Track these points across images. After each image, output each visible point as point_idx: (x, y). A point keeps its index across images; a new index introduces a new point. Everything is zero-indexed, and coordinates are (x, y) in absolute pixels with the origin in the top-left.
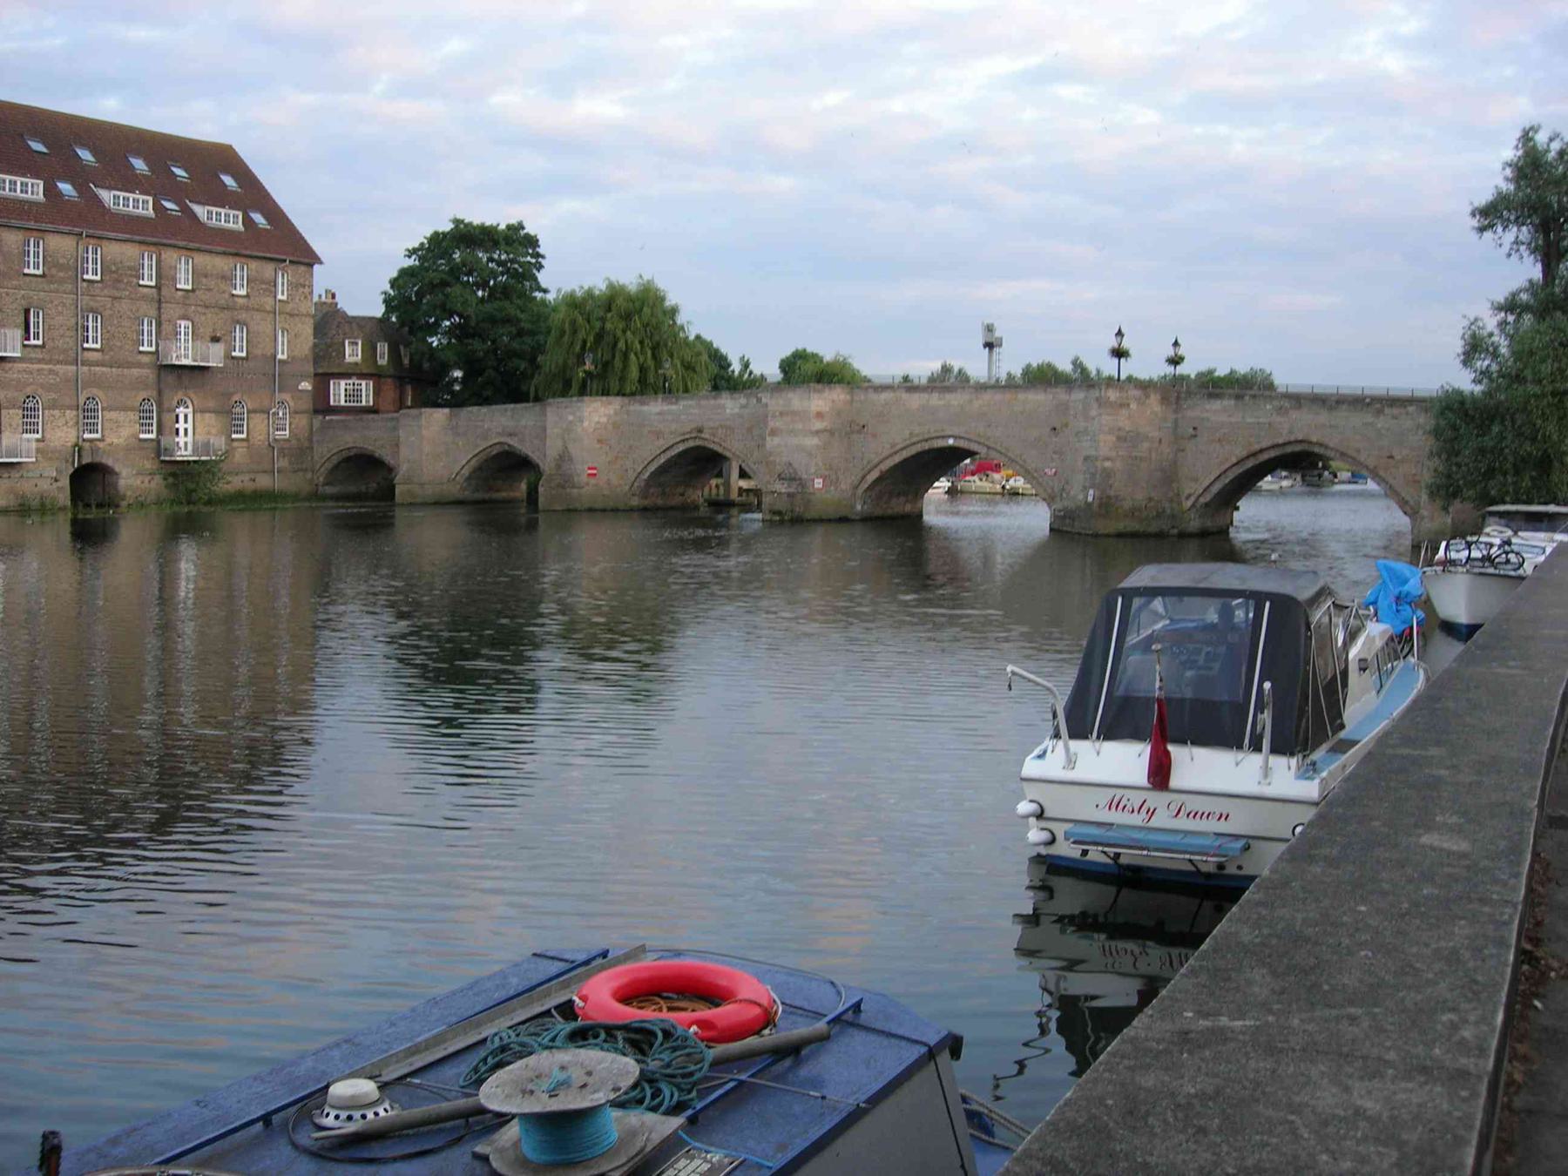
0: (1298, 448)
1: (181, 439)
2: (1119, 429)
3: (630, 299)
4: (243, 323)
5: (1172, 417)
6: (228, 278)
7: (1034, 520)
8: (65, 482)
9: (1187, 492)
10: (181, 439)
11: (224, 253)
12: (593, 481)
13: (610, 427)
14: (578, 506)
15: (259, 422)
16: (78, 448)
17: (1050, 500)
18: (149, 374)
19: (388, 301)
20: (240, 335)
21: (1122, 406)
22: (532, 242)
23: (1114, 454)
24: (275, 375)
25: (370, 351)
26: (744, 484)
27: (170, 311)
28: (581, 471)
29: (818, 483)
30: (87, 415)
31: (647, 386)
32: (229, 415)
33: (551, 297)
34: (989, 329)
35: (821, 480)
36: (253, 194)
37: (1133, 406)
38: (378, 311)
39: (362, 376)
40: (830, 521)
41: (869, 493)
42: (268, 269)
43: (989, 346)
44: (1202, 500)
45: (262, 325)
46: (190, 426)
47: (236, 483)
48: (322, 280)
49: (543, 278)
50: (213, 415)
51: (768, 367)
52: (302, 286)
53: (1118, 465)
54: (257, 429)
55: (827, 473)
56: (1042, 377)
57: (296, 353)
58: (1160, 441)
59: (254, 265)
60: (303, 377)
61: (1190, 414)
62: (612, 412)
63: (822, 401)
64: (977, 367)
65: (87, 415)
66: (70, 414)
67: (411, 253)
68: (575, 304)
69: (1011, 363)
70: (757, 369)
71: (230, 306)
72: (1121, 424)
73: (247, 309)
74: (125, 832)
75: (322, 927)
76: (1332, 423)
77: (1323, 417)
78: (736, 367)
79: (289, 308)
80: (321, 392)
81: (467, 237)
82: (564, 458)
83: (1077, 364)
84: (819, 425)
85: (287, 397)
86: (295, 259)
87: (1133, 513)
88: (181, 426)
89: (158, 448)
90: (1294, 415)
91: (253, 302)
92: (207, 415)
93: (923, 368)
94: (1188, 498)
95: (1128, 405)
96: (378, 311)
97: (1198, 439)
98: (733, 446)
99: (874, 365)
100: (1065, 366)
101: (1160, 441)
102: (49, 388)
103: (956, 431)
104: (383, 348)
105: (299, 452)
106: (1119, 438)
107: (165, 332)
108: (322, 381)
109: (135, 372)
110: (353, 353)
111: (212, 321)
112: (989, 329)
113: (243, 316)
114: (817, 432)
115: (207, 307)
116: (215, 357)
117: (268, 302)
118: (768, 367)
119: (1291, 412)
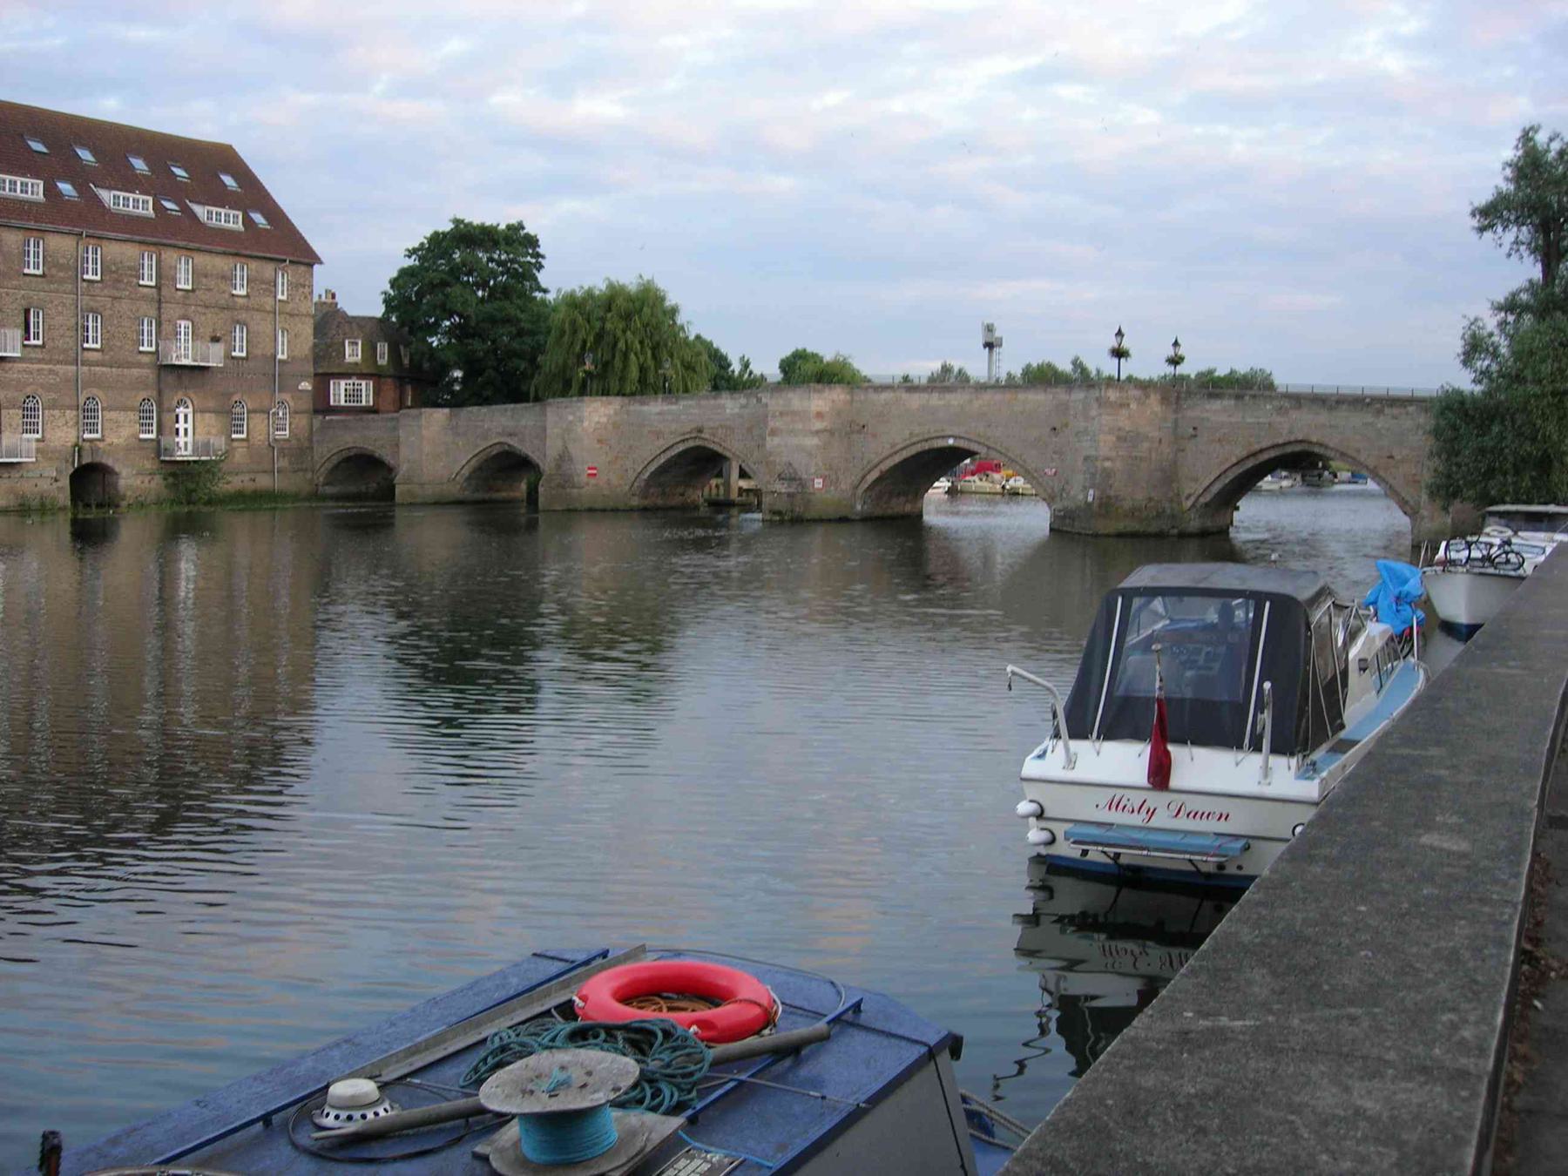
0: (1298, 448)
1: (181, 439)
2: (1119, 429)
3: (630, 299)
4: (243, 323)
5: (1172, 417)
6: (228, 278)
7: (1034, 520)
8: (65, 482)
9: (1187, 492)
10: (181, 439)
11: (224, 253)
12: (593, 481)
13: (610, 427)
14: (578, 506)
15: (259, 422)
16: (78, 448)
17: (1050, 500)
18: (149, 374)
19: (388, 301)
20: (240, 335)
21: (1122, 406)
22: (532, 242)
23: (1114, 454)
24: (275, 375)
25: (370, 351)
26: (744, 484)
27: (170, 311)
28: (581, 471)
29: (818, 483)
30: (87, 415)
31: (647, 386)
32: (229, 415)
33: (551, 297)
34: (989, 329)
35: (821, 480)
36: (253, 194)
37: (1133, 406)
38: (378, 311)
39: (362, 376)
40: (830, 521)
41: (869, 493)
42: (268, 269)
43: (989, 346)
44: (1202, 500)
45: (262, 325)
46: (190, 426)
47: (236, 483)
48: (322, 280)
49: (543, 278)
50: (213, 415)
51: (768, 367)
52: (302, 286)
53: (1118, 465)
54: (257, 429)
55: (827, 473)
56: (1042, 377)
57: (296, 353)
58: (1160, 441)
59: (254, 265)
60: (303, 377)
61: (1190, 414)
62: (612, 412)
63: (822, 401)
64: (977, 367)
65: (87, 415)
66: (70, 414)
67: (411, 253)
68: (575, 304)
69: (1011, 363)
70: (757, 369)
71: (230, 306)
72: (1121, 424)
73: (247, 309)
74: (125, 832)
75: (322, 927)
76: (1332, 423)
77: (1323, 417)
78: (736, 367)
79: (289, 308)
80: (321, 392)
81: (467, 237)
82: (564, 458)
83: (1077, 364)
84: (819, 425)
85: (287, 397)
86: (295, 259)
87: (1133, 513)
88: (181, 426)
89: (158, 448)
90: (1294, 415)
91: (253, 302)
92: (207, 415)
93: (923, 368)
94: (1188, 498)
95: (1128, 405)
96: (378, 311)
97: (1198, 439)
98: (733, 446)
99: (874, 365)
100: (1065, 366)
101: (1160, 441)
102: (49, 388)
103: (956, 431)
104: (383, 348)
105: (299, 452)
106: (1119, 438)
107: (165, 332)
108: (322, 381)
109: (135, 372)
110: (353, 353)
111: (212, 321)
112: (989, 329)
113: (243, 316)
114: (817, 432)
115: (207, 307)
116: (215, 357)
117: (268, 302)
118: (768, 367)
119: (1291, 412)
